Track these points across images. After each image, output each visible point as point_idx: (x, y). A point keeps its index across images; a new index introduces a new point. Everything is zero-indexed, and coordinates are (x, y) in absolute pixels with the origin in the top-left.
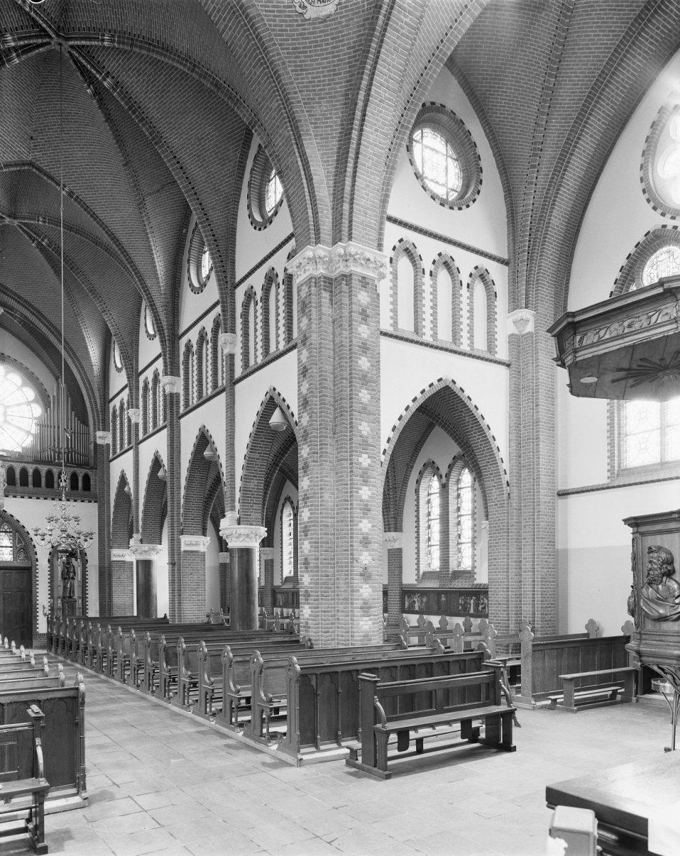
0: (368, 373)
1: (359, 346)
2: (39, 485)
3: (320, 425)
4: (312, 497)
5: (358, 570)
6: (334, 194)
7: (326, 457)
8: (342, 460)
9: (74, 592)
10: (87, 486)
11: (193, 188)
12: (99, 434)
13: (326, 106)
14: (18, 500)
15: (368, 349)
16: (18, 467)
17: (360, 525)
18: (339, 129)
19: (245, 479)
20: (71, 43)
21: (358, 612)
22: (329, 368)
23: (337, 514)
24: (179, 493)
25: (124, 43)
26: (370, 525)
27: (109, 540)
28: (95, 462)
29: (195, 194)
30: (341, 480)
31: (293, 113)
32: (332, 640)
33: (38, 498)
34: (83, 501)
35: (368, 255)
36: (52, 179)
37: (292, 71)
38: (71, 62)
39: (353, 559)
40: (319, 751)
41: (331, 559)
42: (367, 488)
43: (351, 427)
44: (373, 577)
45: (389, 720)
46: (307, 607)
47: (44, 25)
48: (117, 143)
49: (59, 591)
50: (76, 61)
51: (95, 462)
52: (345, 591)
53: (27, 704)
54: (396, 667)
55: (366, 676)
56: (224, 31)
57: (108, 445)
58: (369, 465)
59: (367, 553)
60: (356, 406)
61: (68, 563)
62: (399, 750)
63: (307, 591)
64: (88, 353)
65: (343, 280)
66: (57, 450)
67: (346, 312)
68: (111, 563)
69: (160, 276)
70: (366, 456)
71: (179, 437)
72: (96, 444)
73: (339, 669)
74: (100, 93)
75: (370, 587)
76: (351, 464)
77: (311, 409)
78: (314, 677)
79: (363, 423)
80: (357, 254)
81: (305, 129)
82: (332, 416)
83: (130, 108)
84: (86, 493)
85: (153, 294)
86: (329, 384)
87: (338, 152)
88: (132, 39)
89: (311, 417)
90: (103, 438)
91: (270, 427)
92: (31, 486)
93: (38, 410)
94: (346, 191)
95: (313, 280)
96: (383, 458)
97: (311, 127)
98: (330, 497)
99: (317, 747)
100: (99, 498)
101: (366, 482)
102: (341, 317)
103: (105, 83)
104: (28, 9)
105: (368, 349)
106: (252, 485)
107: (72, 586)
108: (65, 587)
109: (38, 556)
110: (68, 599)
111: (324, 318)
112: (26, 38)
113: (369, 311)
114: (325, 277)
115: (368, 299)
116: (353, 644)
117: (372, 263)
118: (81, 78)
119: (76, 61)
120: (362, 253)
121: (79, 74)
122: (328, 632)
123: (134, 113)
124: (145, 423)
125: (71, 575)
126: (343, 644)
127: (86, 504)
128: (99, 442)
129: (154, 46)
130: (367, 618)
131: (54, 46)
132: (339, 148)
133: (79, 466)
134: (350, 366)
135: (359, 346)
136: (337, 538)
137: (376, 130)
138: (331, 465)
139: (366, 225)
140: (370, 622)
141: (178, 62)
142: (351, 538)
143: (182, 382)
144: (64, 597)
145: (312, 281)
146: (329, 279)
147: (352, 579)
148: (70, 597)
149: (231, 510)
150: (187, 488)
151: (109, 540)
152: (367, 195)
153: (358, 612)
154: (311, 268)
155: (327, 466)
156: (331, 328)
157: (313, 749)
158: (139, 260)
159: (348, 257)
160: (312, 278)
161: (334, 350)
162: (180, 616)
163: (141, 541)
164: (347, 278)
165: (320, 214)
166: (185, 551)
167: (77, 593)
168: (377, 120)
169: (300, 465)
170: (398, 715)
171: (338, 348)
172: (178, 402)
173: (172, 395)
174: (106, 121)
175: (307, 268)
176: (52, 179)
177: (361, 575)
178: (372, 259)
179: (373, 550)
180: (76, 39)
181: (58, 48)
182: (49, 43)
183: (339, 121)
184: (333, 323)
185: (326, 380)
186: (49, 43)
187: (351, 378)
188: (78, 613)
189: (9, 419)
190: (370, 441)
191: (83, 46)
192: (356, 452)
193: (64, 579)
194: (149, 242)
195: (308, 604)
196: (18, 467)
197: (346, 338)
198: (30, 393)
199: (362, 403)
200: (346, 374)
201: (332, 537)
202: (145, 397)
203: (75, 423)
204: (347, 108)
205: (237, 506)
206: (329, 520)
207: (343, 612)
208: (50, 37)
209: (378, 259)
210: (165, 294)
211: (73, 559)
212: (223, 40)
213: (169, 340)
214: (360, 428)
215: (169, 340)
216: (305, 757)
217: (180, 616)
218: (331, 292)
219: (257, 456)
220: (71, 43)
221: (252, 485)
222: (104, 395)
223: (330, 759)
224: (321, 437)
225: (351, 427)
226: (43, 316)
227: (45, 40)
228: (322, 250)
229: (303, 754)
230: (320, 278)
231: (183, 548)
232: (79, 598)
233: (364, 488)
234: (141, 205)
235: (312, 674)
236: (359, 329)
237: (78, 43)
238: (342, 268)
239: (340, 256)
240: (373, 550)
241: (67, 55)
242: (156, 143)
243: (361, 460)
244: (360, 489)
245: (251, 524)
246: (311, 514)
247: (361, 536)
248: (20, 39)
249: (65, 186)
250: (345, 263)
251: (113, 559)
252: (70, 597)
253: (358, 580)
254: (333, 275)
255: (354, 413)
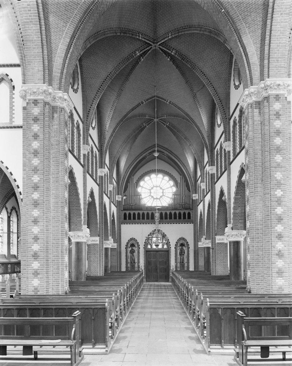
0: (281, 145)
1: (275, 133)
2: (149, 219)
3: (254, 177)
4: (250, 215)
5: (275, 252)
6: (260, 57)
7: (257, 193)
8: (265, 194)
9: (184, 260)
10: (189, 217)
11: (210, 82)
12: (194, 195)
13: (254, 15)
14: (164, 225)
15: (280, 133)
16: (164, 212)
17: (276, 228)
18: (261, 23)
19: (235, 208)
20: (158, 44)
21: (275, 275)
22: (259, 148)
23: (264, 223)
24: (215, 217)
25: (175, 34)
26: (283, 228)
27: (198, 239)
28: (192, 207)
29: (211, 84)
30: (265, 205)
31: (237, 27)
32: (261, 289)
33: (171, 224)
34: (187, 223)
35: (278, 83)
36: (163, 99)
37: (236, 7)
38: (160, 51)
39: (272, 246)
40: (223, 348)
41: (261, 247)
42: (280, 208)
43: (270, 176)
44: (285, 256)
45: (249, 339)
46: (249, 271)
47: (148, 42)
48: (182, 75)
49: (179, 261)
50: (162, 50)
51: (192, 207)
52: (268, 263)
53: (76, 309)
54: (275, 308)
55: (240, 313)
56: (204, 6)
57: (197, 199)
58: (282, 195)
59: (281, 243)
60: (273, 165)
61: (182, 249)
62: (262, 357)
63: (249, 263)
64: (188, 163)
65: (265, 100)
66: (180, 204)
67: (267, 117)
68: (198, 248)
69: (205, 124)
70: (280, 190)
71: (215, 193)
72: (192, 199)
73: (263, 307)
74: (173, 59)
75: (283, 261)
76: (270, 196)
77: (249, 170)
78: (220, 310)
79: (278, 173)
80: (271, 84)
81: (243, 32)
82: (261, 172)
83: (182, 59)
84: (189, 220)
85: (203, 133)
86: (259, 156)
87: (262, 35)
88: (129, 31)
89: (249, 174)
90: (195, 197)
91: (242, 182)
92: (168, 219)
93: (174, 189)
94: (265, 53)
95: (250, 105)
96: (21, 197)
97: (247, 30)
98: (260, 214)
99: (222, 346)
100: (194, 222)
101: (279, 204)
102: (264, 120)
103: (172, 53)
104: (141, 39)
105: (280, 133)
106: (238, 211)
107: (183, 258)
108: (181, 259)
109: (171, 246)
110: (182, 263)
111: (255, 123)
112: (143, 50)
113: (280, 113)
114: (256, 102)
115: (281, 106)
116: (272, 292)
117: (282, 86)
118: (165, 56)
119: (162, 50)
120: (275, 83)
121: (164, 54)
122: (259, 285)
123: (184, 60)
124: (206, 188)
125: (183, 253)
126: (267, 292)
127: (189, 224)
128: (194, 198)
129: (186, 28)
130: (281, 278)
131: (154, 48)
132: (262, 33)
133: (186, 209)
134: (270, 144)
135: (275, 133)
136: (264, 236)
137: (282, 14)
138: (260, 197)
139: (279, 67)
140: (283, 281)
141: (195, 30)
142: (271, 235)
143: (216, 168)
144: (180, 262)
145: (251, 105)
146: (258, 102)
147: (272, 257)
148: (182, 262)
149: (229, 223)
150: (218, 214)
151: (198, 239)
152: (278, 50)
153: (275, 275)
154: (248, 100)
155: (258, 198)
156: (260, 127)
157: (220, 347)
158: (196, 120)
159: (267, 87)
160: (249, 104)
161: (262, 138)
162: (215, 272)
163: (206, 239)
164: (267, 98)
165: (252, 71)
166: (218, 243)
167: (185, 260)
168: (281, 8)
169: (246, 199)
170: (276, 336)
171: (263, 135)
172: (214, 177)
173: (212, 175)
174: (177, 68)
175: (246, 100)
176: (163, 99)
177: (277, 255)
178: (281, 83)
179: (285, 241)
180: (160, 41)
181: (155, 48)
182: (151, 48)
183: (261, 19)
184: (261, 124)
185: (257, 154)
186: (151, 48)
187: (270, 150)
188: (186, 269)
189: (164, 194)
190: (282, 182)
191: (163, 43)
192: (273, 189)
193: (180, 255)
194: (199, 111)
195: (249, 270)
196: (164, 212)
197: (267, 130)
198: (172, 183)
199: (277, 162)
200: (267, 149)
201: (261, 235)
202: (206, 177)
203: (187, 191)
204: (265, 10)
205: (232, 221)
206: (259, 226)
207: (266, 274)
208: (151, 45)
209: (285, 82)
210: (207, 131)
211: (184, 247)
212: (204, 10)
213: (210, 151)
214: (275, 176)
215: (210, 151)
216: (212, 351)
217: (215, 272)
218: (260, 108)
219: (239, 197)
220: (158, 44)
221: (238, 211)
222: (195, 179)
223: (228, 354)
224: (255, 184)
225: (270, 176)
226: (173, 153)
227: (150, 47)
228: (252, 89)
229: (211, 349)
230: (253, 103)
231: (217, 241)
232: (186, 262)
233: (279, 208)
234: (194, 97)
235: (219, 308)
236: (275, 123)
237: (161, 42)
238: (265, 94)
239: (262, 88)
240: (285, 241)
241: (158, 49)
242: (193, 69)
243: (276, 193)
244: (276, 209)
245: (238, 230)
246: (250, 224)
247: (277, 234)
248: (141, 51)
249: (168, 100)
250: (265, 91)
251: (199, 246)
252: (182, 262)
253: (274, 258)
254: (260, 100)
255: (271, 168)
